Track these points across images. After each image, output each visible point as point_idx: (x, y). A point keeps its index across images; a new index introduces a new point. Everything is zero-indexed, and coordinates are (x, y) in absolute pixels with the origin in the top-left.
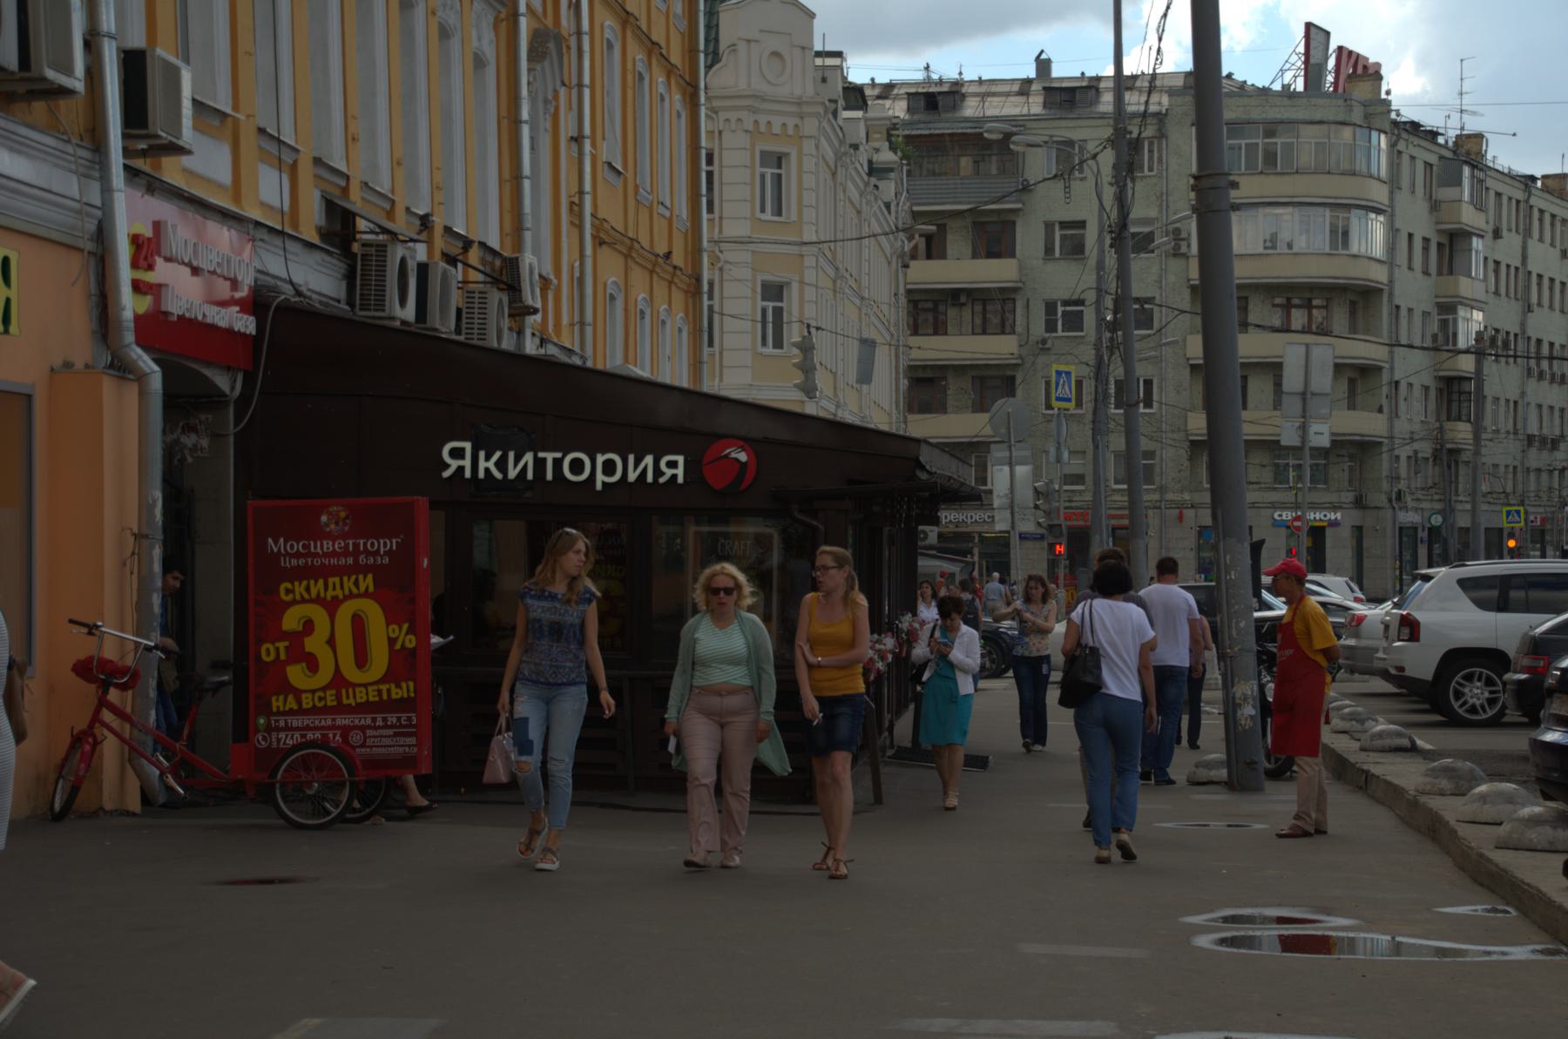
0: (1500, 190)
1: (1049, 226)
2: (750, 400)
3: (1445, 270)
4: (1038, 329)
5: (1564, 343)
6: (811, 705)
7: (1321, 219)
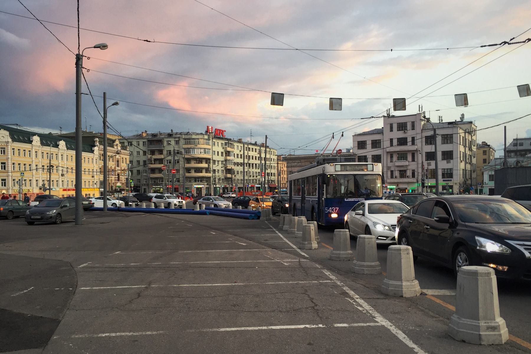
0: (256, 148)
1: (167, 151)
2: (529, 138)
3: (395, 231)
4: (166, 163)
5: (383, 127)
6: (243, 166)
7: (200, 140)
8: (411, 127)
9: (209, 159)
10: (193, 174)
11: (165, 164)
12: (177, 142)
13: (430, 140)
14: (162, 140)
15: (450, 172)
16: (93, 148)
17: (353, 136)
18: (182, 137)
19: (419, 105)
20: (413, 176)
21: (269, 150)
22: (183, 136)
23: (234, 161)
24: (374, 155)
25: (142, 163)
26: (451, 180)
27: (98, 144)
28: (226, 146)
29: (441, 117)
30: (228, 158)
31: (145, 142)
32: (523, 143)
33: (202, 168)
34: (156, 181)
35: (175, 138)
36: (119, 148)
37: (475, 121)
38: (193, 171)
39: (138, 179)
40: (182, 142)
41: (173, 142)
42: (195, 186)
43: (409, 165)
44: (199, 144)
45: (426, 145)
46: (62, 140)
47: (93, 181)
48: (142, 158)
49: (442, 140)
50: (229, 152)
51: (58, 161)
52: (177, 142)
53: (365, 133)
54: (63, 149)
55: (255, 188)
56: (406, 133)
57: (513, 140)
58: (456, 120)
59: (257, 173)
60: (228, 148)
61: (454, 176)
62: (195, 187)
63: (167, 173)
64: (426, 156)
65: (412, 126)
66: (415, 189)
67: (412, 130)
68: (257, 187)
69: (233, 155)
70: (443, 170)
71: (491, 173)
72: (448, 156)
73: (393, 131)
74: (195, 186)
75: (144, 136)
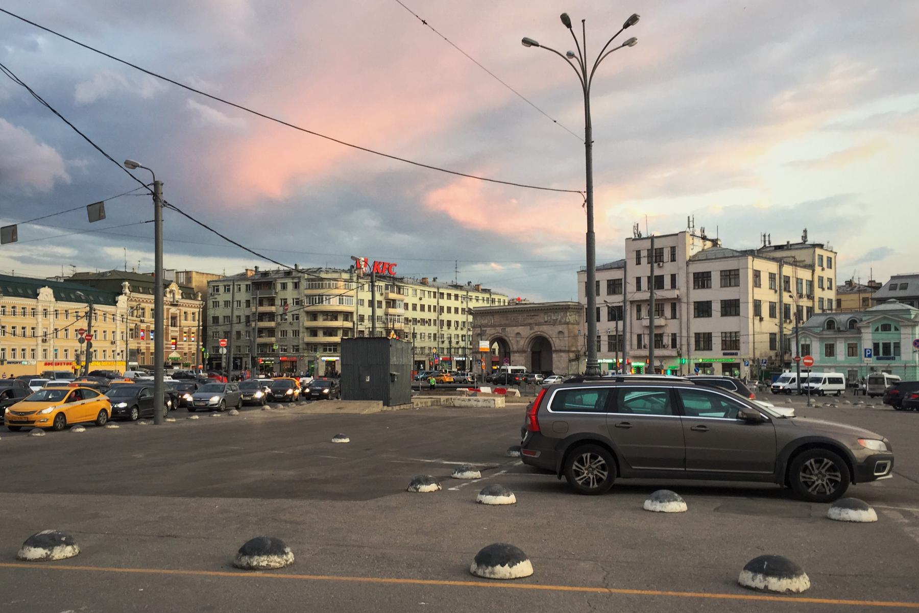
2: (912, 274)
8: (670, 255)
9: (352, 313)
10: (321, 339)
11: (277, 320)
12: (296, 286)
13: (701, 280)
14: (273, 282)
15: (734, 339)
16: (116, 298)
17: (578, 272)
18: (304, 277)
19: (689, 217)
20: (674, 345)
21: (489, 297)
22: (306, 276)
23: (405, 316)
24: (725, 300)
25: (243, 319)
26: (736, 354)
27: (127, 291)
28: (387, 291)
29: (767, 235)
30: (391, 311)
31: (250, 285)
32: (908, 284)
33: (337, 329)
34: (265, 350)
35: (293, 278)
36: (178, 297)
37: (828, 243)
38: (320, 333)
39: (237, 346)
40: (304, 284)
41: (290, 286)
42: (323, 358)
43: (666, 325)
44: (329, 287)
45: (694, 288)
46: (45, 287)
47: (114, 349)
48: (243, 312)
49: (721, 279)
50: (394, 301)
51: (37, 319)
52: (296, 286)
53: (606, 267)
54: (48, 300)
55: (454, 364)
56: (661, 267)
57: (890, 279)
58: (788, 242)
59: (458, 337)
60: (390, 294)
61: (742, 346)
62: (323, 361)
63: (281, 336)
64: (694, 309)
65: (671, 255)
66: (676, 369)
67: (671, 261)
68: (457, 362)
69: (402, 305)
70: (724, 335)
71: (806, 341)
72: (731, 308)
73: (640, 264)
74: (323, 358)
75: (249, 276)
